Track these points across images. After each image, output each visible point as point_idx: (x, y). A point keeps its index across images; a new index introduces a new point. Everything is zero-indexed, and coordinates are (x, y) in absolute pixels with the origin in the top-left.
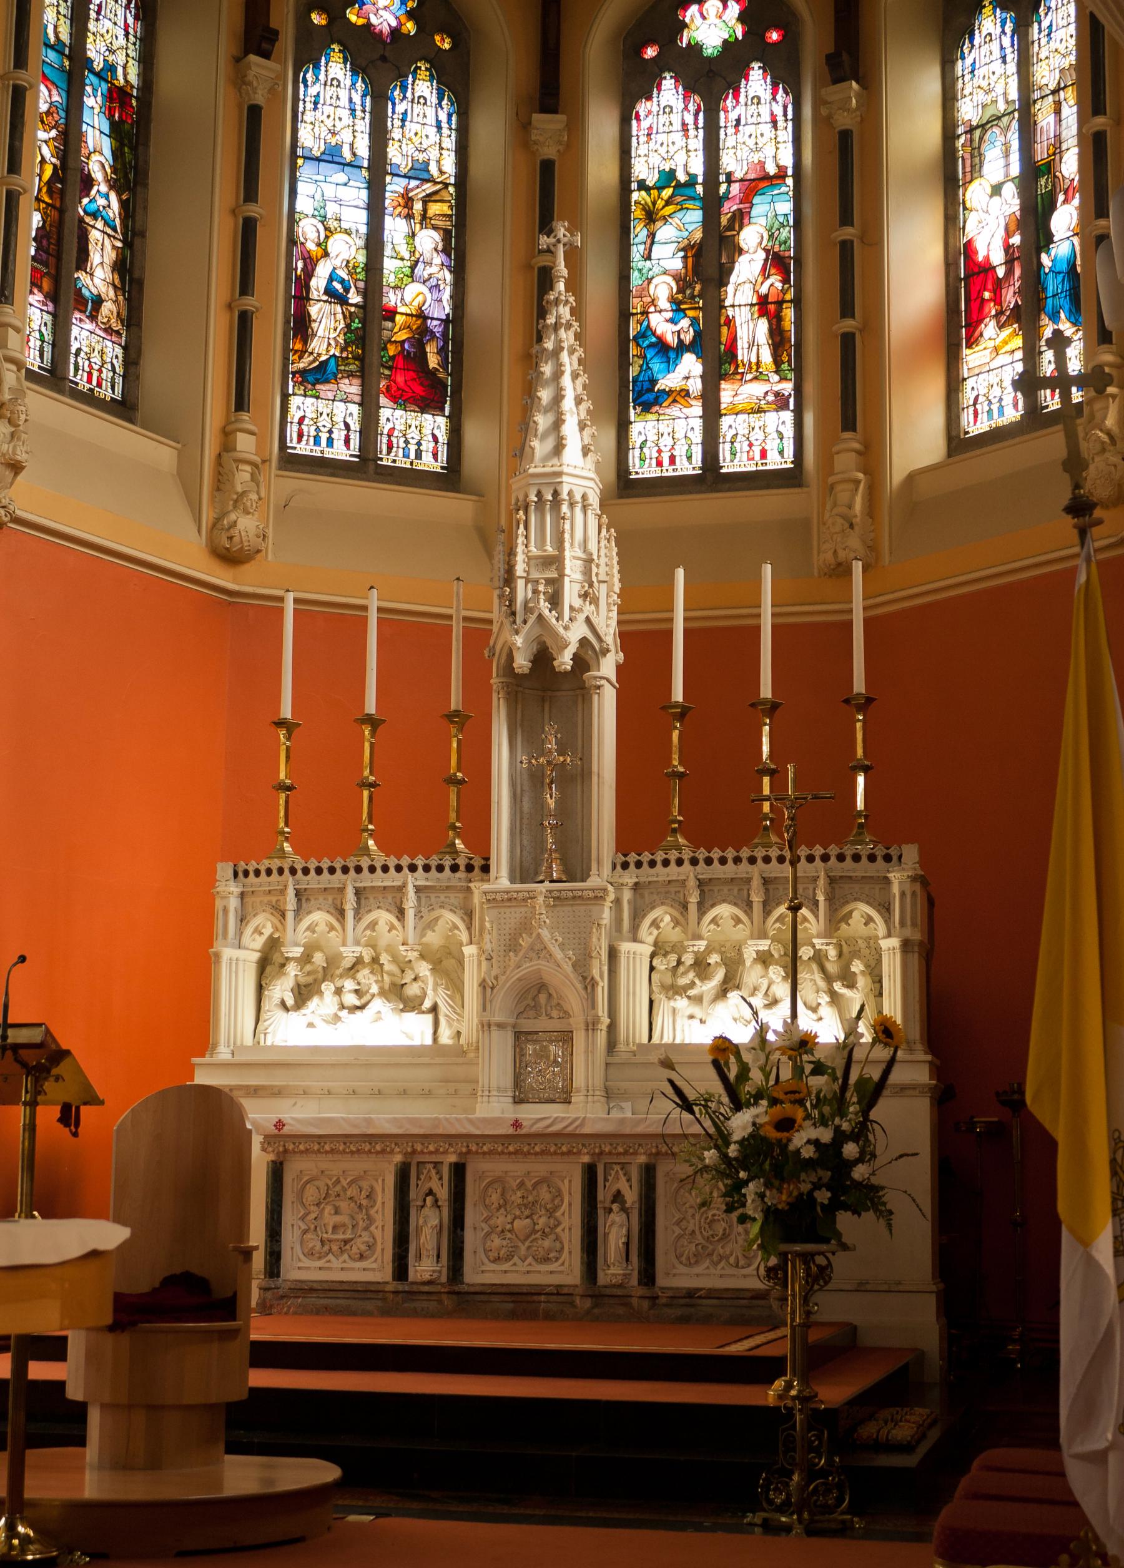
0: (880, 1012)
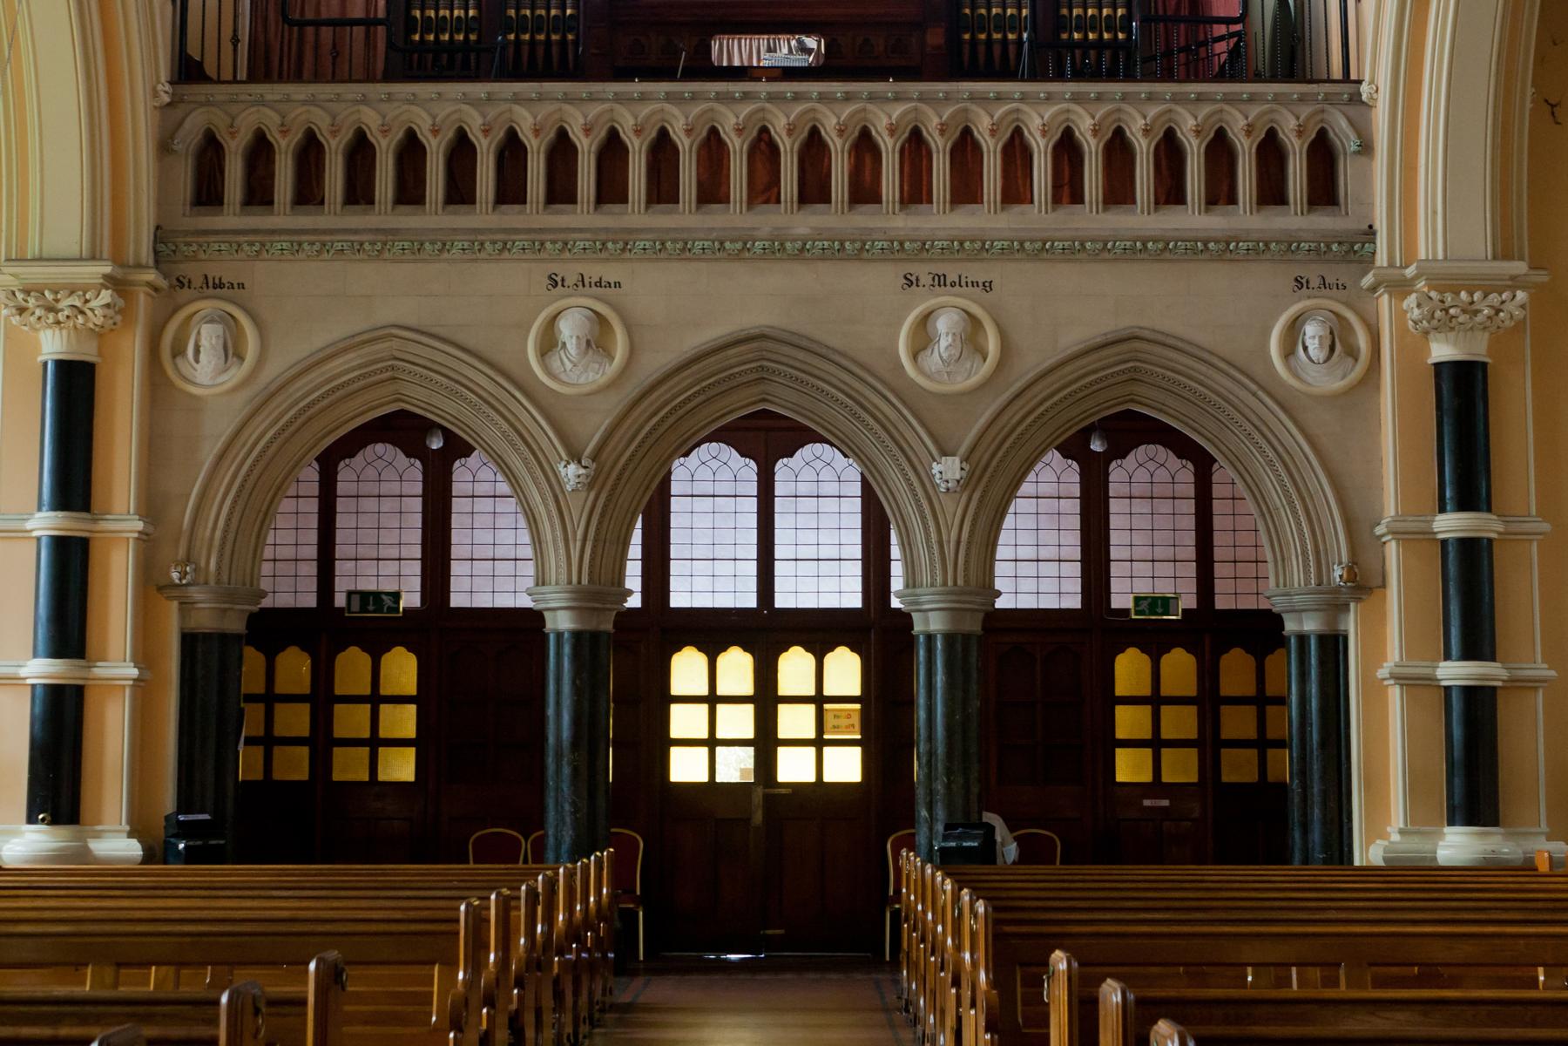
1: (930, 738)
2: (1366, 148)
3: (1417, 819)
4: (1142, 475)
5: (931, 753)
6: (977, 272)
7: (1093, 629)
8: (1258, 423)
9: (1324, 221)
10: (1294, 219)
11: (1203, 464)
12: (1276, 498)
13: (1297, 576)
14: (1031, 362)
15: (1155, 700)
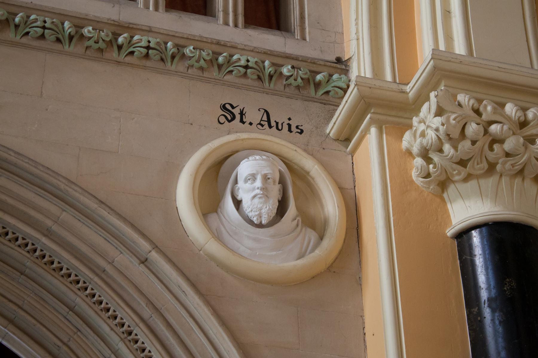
8: (147, 312)
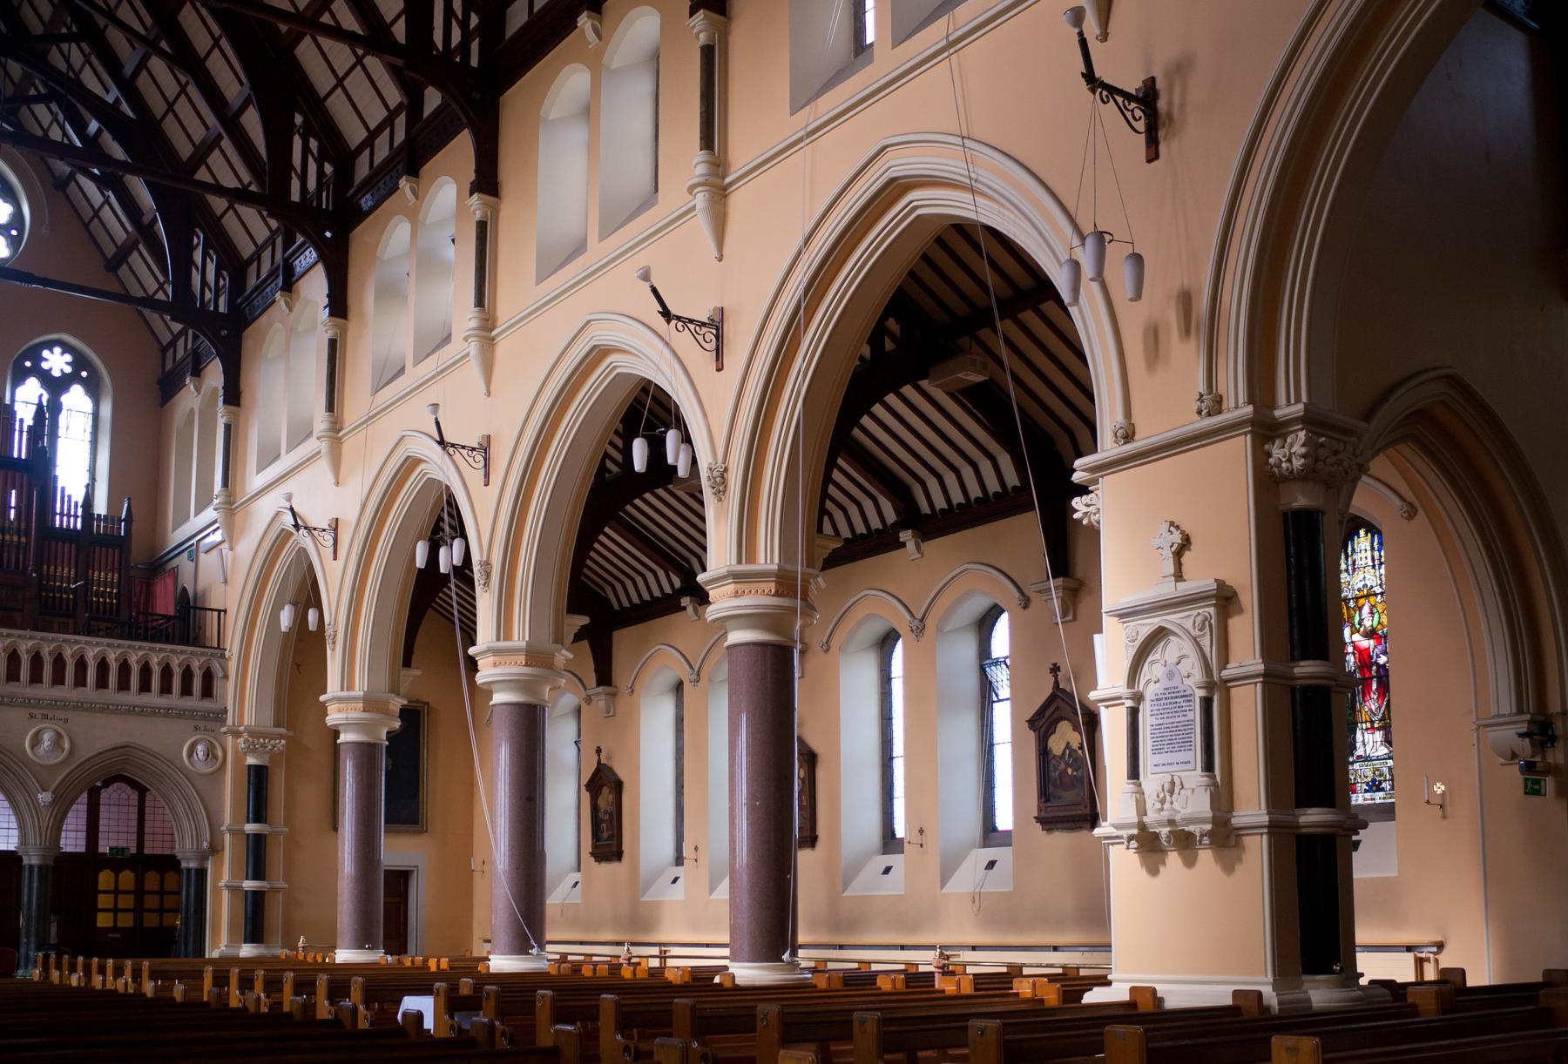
0: (1056, 683)
1: (29, 908)
2: (226, 677)
3: (233, 940)
4: (115, 796)
5: (29, 915)
6: (62, 714)
7: (91, 860)
9: (207, 704)
10: (195, 702)
11: (142, 791)
12: (181, 813)
13: (188, 846)
14: (83, 755)
15: (116, 892)
